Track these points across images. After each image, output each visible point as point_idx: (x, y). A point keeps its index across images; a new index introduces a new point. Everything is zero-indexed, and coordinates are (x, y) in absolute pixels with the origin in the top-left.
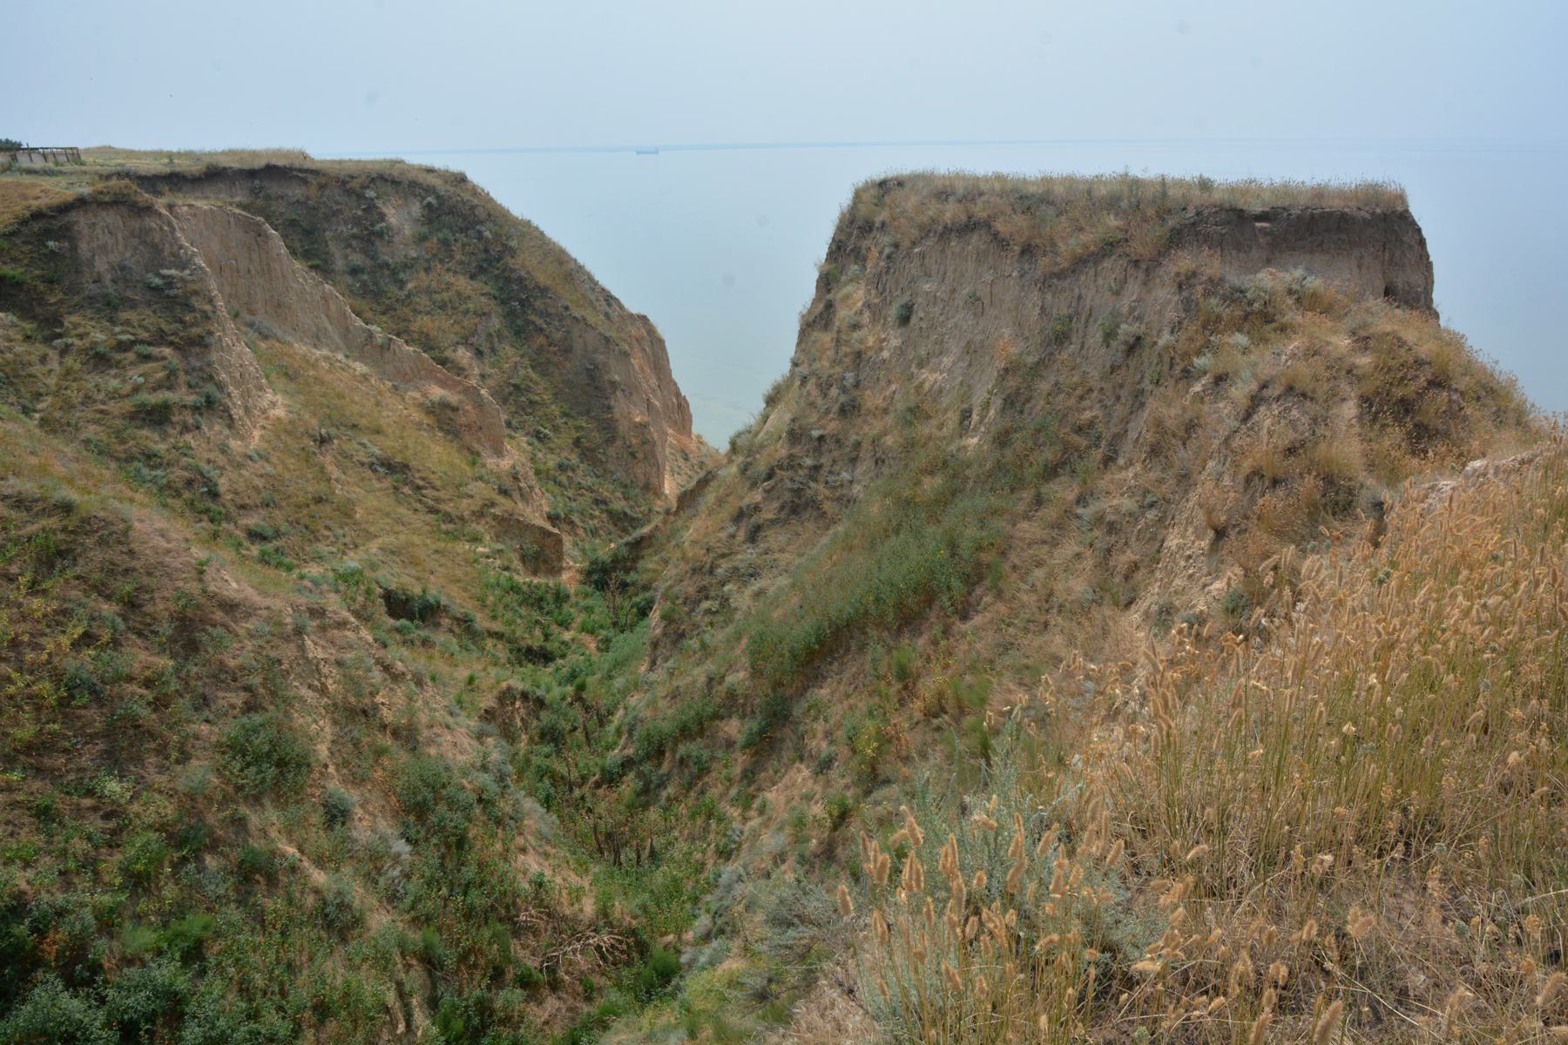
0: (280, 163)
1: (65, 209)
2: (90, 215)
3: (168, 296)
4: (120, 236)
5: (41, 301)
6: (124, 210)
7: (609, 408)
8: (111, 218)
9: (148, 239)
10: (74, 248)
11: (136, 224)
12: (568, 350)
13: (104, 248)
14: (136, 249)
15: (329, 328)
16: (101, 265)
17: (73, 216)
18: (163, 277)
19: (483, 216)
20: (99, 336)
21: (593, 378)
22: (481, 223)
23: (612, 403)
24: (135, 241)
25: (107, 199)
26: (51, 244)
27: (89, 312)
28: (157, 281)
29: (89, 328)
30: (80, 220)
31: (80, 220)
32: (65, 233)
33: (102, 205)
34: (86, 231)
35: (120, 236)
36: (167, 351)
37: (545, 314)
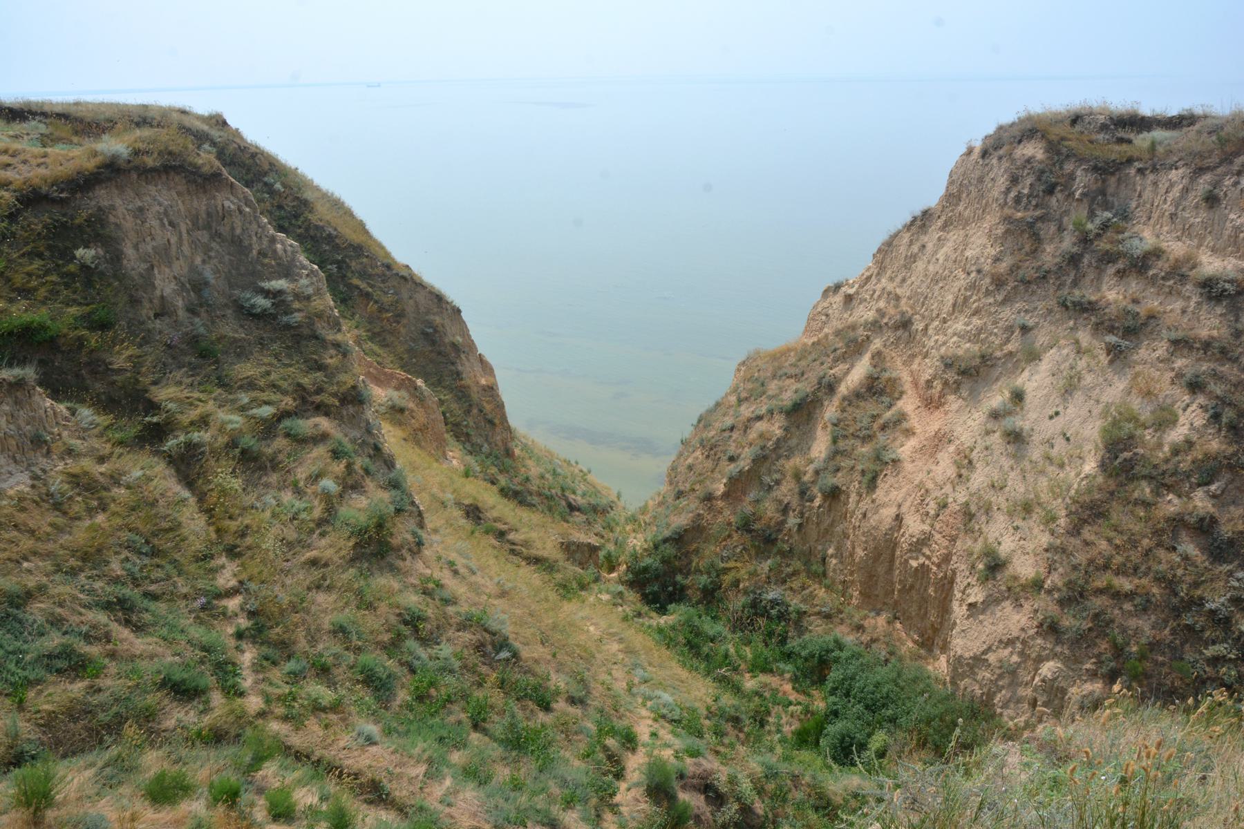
0: (16, 107)
1: (83, 183)
2: (130, 193)
3: (288, 327)
4: (183, 228)
5: (99, 368)
6: (179, 180)
7: (458, 374)
8: (163, 197)
9: (224, 230)
10: (116, 258)
11: (201, 204)
12: (400, 316)
13: (165, 254)
14: (207, 249)
15: (40, 315)
16: (165, 285)
17: (103, 196)
18: (267, 293)
19: (266, 167)
20: (235, 420)
21: (433, 343)
22: (266, 174)
23: (460, 368)
24: (203, 236)
25: (150, 161)
26: (80, 252)
27: (178, 374)
28: (262, 302)
29: (210, 406)
30: (117, 203)
31: (117, 203)
32: (96, 229)
33: (147, 174)
34: (129, 223)
35: (183, 228)
36: (324, 423)
37: (363, 275)
